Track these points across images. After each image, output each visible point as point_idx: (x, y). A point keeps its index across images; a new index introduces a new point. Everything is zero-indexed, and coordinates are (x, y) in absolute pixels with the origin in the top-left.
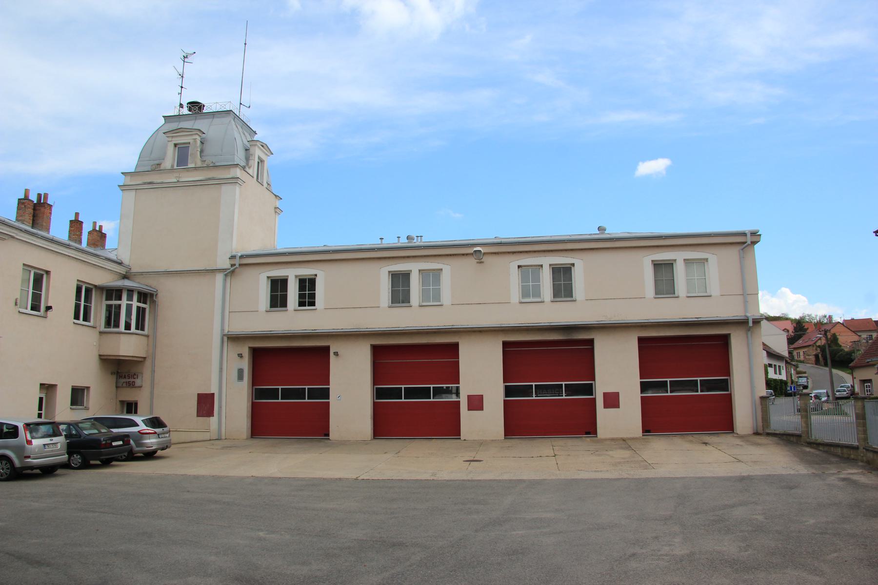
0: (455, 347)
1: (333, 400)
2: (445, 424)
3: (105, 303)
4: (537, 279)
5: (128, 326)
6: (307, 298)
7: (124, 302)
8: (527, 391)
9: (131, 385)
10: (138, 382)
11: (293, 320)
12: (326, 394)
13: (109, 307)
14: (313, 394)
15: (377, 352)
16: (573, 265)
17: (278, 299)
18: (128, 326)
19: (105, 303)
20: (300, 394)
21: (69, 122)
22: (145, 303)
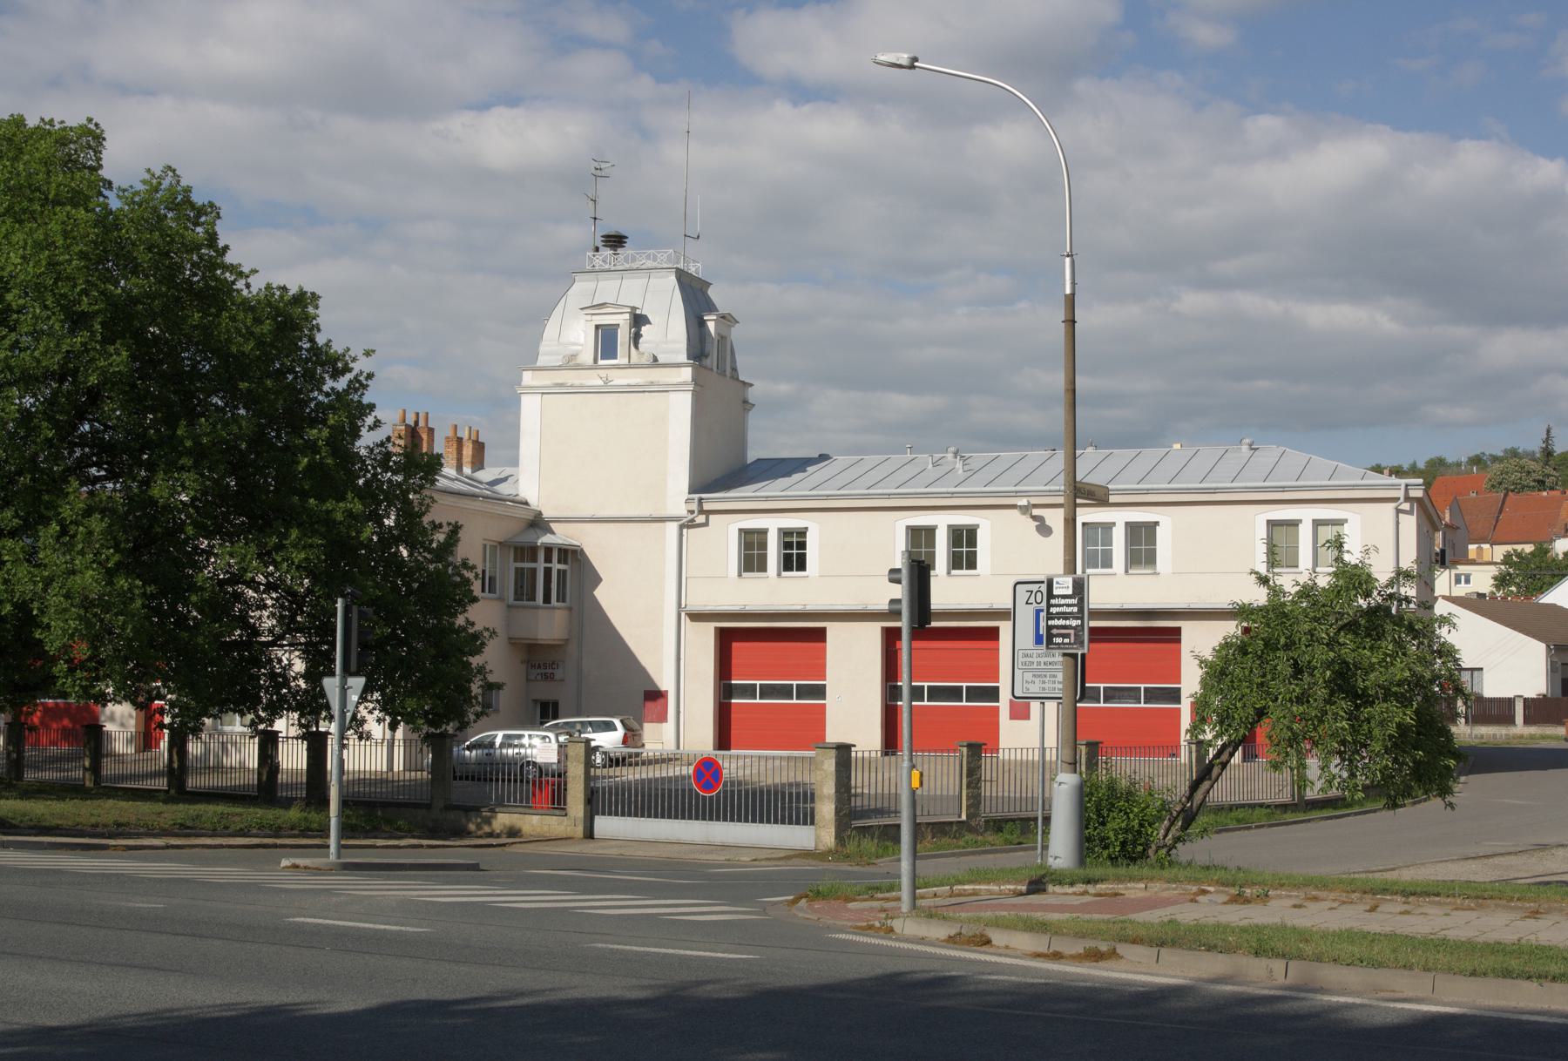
0: (820, 635)
1: (830, 701)
2: (785, 533)
3: (513, 565)
4: (1108, 541)
5: (547, 599)
6: (794, 559)
7: (541, 565)
8: (1152, 695)
9: (548, 677)
10: (558, 674)
11: (773, 592)
12: (820, 692)
13: (519, 572)
14: (804, 692)
15: (726, 639)
16: (1157, 523)
17: (752, 559)
18: (547, 599)
19: (513, 565)
20: (785, 692)
21: (164, 114)
22: (565, 562)
